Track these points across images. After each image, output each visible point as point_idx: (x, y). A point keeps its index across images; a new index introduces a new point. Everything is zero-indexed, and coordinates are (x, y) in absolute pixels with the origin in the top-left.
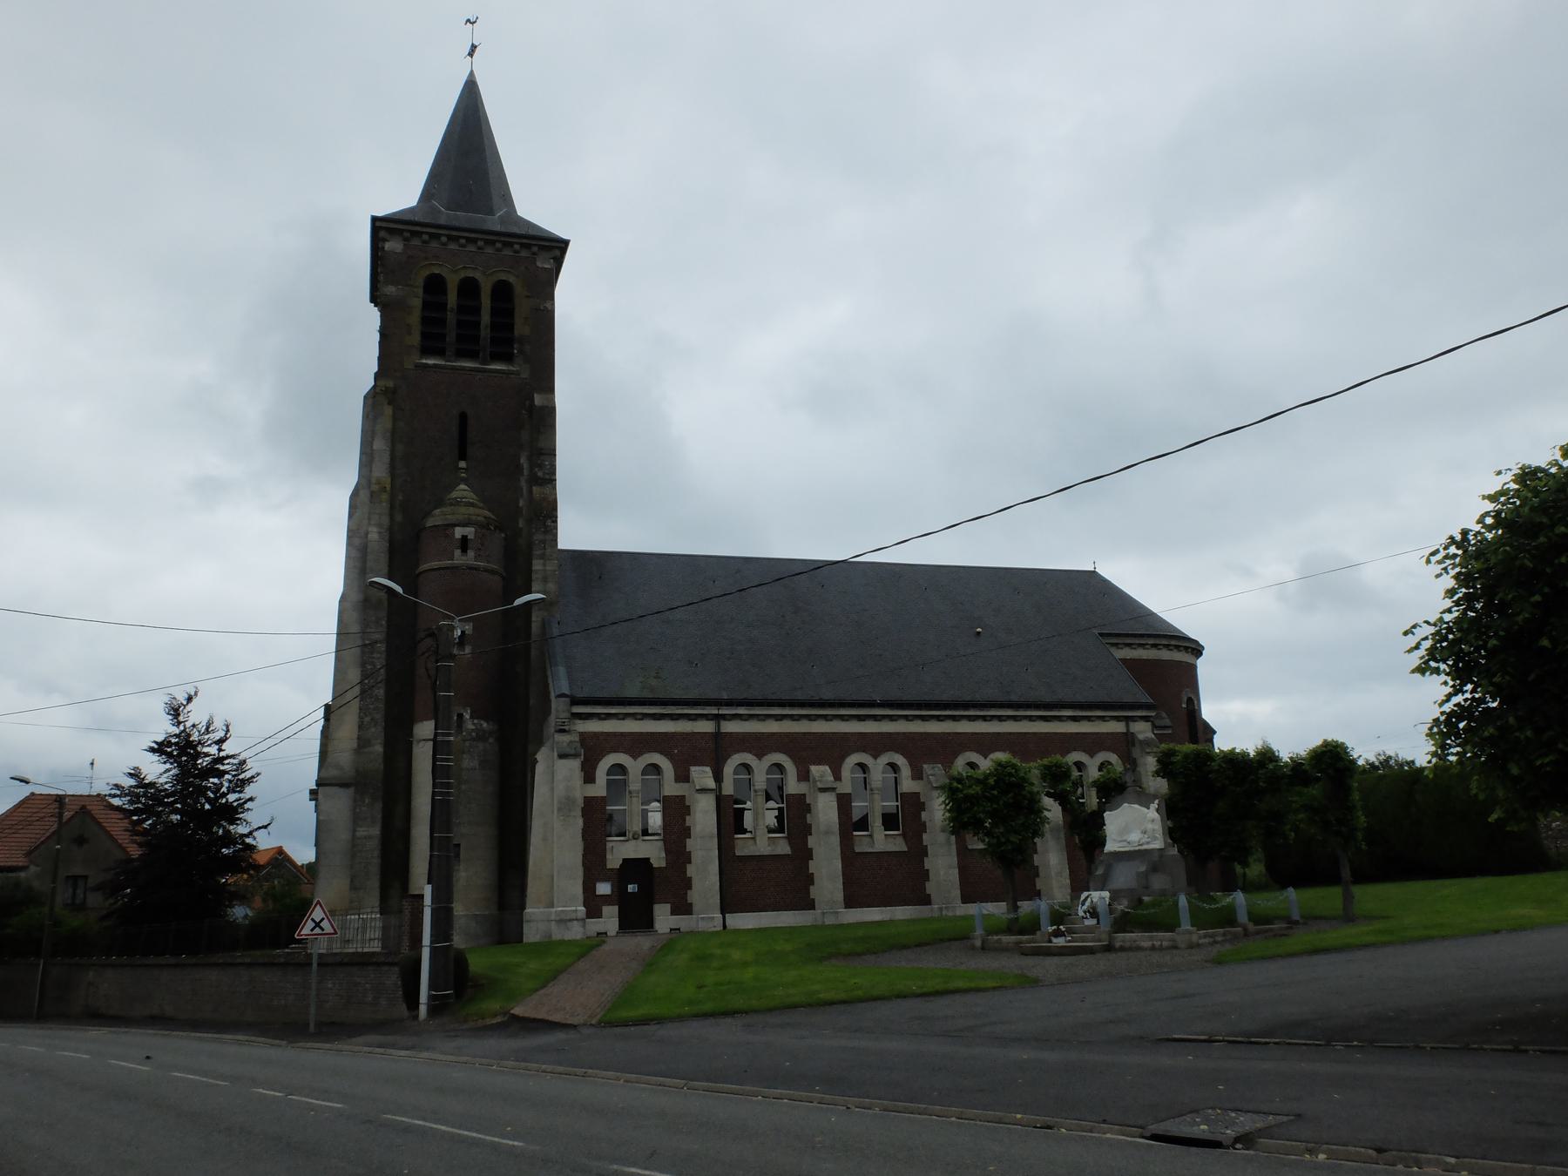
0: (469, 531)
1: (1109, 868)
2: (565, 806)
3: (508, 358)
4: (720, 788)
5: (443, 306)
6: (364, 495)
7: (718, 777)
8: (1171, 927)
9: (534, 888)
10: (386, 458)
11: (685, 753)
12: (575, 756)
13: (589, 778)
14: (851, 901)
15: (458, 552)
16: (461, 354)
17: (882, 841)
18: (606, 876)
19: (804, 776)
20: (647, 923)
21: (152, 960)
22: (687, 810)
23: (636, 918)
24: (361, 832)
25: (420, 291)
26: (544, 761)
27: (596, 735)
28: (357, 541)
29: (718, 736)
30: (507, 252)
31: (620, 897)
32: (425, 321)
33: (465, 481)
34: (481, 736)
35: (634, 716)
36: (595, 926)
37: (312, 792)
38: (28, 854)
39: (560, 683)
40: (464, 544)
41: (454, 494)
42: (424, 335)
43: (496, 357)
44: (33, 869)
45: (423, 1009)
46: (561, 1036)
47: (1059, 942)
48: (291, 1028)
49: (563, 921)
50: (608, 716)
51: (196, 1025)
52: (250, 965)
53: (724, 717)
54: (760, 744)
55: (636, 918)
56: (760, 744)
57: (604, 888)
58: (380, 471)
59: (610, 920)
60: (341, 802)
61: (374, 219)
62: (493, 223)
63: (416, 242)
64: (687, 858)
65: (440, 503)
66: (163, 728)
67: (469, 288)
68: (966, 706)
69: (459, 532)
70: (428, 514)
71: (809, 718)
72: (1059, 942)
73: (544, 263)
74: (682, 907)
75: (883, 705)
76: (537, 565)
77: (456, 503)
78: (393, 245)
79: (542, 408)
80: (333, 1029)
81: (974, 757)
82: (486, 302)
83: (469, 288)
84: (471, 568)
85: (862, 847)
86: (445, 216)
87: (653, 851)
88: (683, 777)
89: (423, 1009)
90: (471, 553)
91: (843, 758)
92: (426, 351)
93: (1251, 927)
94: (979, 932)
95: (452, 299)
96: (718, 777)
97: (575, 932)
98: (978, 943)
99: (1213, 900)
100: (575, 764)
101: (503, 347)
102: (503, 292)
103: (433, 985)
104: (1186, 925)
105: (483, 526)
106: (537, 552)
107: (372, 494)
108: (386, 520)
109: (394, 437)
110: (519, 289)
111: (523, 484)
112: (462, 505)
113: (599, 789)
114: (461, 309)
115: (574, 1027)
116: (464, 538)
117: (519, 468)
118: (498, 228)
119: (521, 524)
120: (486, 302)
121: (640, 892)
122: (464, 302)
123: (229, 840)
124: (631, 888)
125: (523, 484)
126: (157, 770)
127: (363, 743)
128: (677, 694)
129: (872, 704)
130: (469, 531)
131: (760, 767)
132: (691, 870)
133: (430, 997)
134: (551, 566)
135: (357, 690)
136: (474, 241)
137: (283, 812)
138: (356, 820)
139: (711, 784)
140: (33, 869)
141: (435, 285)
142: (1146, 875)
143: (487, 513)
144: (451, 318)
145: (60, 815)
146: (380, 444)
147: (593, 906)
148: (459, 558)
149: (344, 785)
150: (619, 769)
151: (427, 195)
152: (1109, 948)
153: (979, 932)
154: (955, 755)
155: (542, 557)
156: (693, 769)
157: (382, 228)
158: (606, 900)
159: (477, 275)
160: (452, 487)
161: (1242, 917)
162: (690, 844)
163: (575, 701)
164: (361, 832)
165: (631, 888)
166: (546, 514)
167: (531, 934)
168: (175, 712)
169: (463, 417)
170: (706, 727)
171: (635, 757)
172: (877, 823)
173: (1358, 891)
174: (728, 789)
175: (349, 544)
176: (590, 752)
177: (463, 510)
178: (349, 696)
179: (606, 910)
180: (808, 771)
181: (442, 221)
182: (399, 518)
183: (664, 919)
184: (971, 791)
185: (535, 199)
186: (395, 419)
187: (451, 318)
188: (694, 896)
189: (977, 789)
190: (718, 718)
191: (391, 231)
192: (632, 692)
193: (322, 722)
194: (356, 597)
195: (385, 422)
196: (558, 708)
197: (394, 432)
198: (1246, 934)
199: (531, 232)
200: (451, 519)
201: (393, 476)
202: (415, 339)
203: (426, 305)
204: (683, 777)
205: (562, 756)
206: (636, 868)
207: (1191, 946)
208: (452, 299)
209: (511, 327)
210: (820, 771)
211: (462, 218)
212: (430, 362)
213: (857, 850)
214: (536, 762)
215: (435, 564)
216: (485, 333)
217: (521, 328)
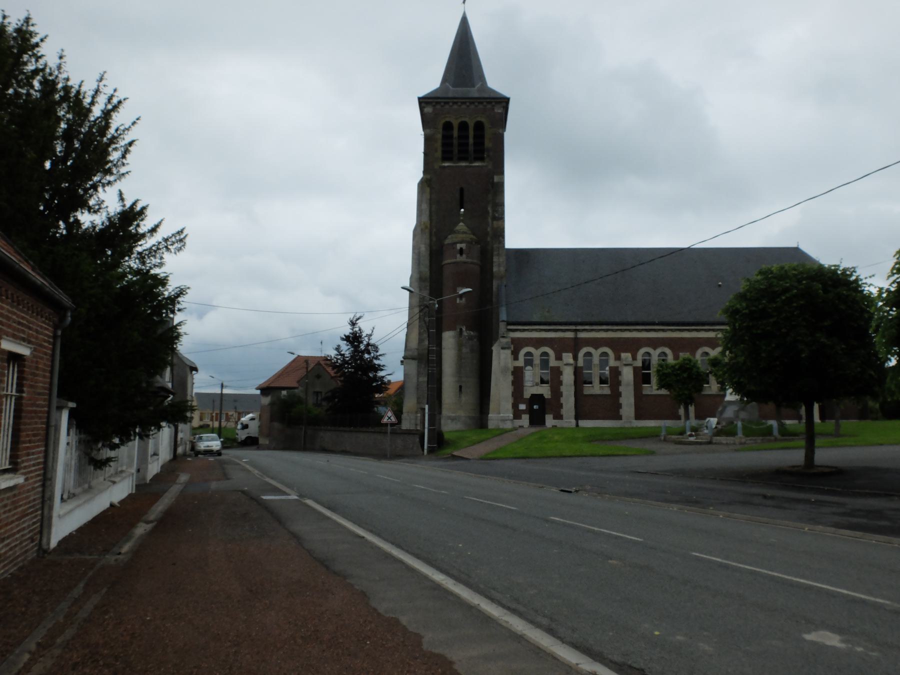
0: (463, 246)
1: (725, 408)
2: (504, 370)
3: (482, 159)
4: (576, 363)
5: (451, 137)
6: (419, 230)
7: (575, 358)
8: (734, 434)
9: (492, 406)
10: (428, 213)
11: (560, 347)
12: (508, 348)
13: (516, 358)
14: (638, 417)
15: (458, 255)
16: (461, 159)
17: (596, 389)
18: (523, 401)
19: (618, 358)
20: (542, 422)
21: (342, 428)
22: (561, 373)
23: (537, 420)
24: (421, 379)
25: (441, 130)
26: (495, 349)
27: (519, 338)
28: (417, 251)
29: (576, 339)
30: (481, 106)
31: (530, 411)
32: (444, 145)
33: (462, 221)
34: (470, 338)
35: (536, 330)
36: (518, 423)
37: (402, 362)
38: (298, 382)
39: (503, 316)
40: (461, 251)
41: (458, 228)
42: (444, 152)
43: (477, 159)
44: (300, 388)
45: (426, 451)
46: (462, 462)
47: (692, 439)
48: (381, 456)
49: (504, 420)
50: (524, 330)
51: (356, 454)
52: (374, 432)
53: (578, 330)
54: (596, 343)
55: (537, 420)
56: (596, 343)
57: (522, 407)
58: (426, 218)
59: (525, 420)
60: (413, 364)
61: (419, 99)
62: (474, 92)
63: (438, 107)
64: (561, 394)
65: (452, 232)
66: (347, 330)
67: (463, 126)
68: (703, 324)
69: (459, 246)
70: (446, 238)
71: (621, 330)
72: (692, 439)
73: (499, 110)
74: (558, 416)
75: (658, 324)
76: (495, 259)
77: (459, 232)
78: (429, 110)
79: (498, 183)
80: (396, 456)
81: (707, 349)
82: (471, 133)
83: (463, 126)
84: (465, 263)
85: (588, 390)
86: (453, 91)
87: (545, 391)
88: (559, 358)
89: (426, 451)
90: (464, 256)
91: (638, 350)
92: (444, 159)
93: (779, 437)
94: (663, 433)
95: (455, 133)
96: (575, 358)
97: (508, 425)
98: (662, 438)
99: (763, 424)
100: (509, 352)
101: (480, 153)
102: (479, 126)
103: (429, 442)
104: (740, 434)
105: (469, 243)
106: (495, 253)
107: (422, 230)
108: (428, 241)
109: (431, 202)
110: (487, 125)
111: (490, 220)
112: (461, 234)
113: (520, 363)
114: (460, 137)
115: (467, 459)
116: (461, 249)
117: (488, 212)
118: (476, 95)
119: (489, 239)
120: (471, 133)
121: (539, 410)
122: (465, 132)
123: (375, 379)
124: (535, 407)
125: (490, 220)
126: (346, 349)
127: (421, 341)
128: (556, 319)
129: (654, 324)
130: (463, 246)
131: (596, 354)
132: (563, 400)
133: (428, 447)
134: (502, 259)
135: (418, 316)
136: (464, 103)
137: (393, 368)
138: (419, 374)
139: (571, 361)
140: (300, 388)
141: (448, 126)
142: (738, 411)
143: (472, 236)
144: (455, 142)
145: (307, 368)
146: (425, 206)
147: (517, 415)
148: (459, 258)
149: (413, 359)
150: (529, 354)
151: (445, 80)
152: (710, 443)
153: (663, 433)
154: (697, 348)
155: (498, 255)
156: (564, 354)
157: (424, 102)
158: (523, 412)
159: (467, 120)
160: (457, 224)
161: (776, 432)
162: (621, 389)
163: (509, 324)
164: (421, 379)
165: (535, 407)
166: (500, 234)
167: (491, 425)
168: (353, 324)
169: (462, 190)
170: (570, 335)
171: (537, 349)
172: (596, 381)
173: (843, 423)
174: (581, 363)
175: (413, 252)
176: (516, 346)
177: (460, 236)
178: (415, 318)
179: (523, 416)
180: (620, 356)
181: (450, 95)
182: (434, 239)
183: (550, 421)
184: (666, 371)
185: (496, 79)
186: (431, 194)
187: (455, 142)
188: (564, 411)
189: (669, 371)
190: (576, 331)
191: (427, 103)
192: (535, 318)
193: (406, 330)
194: (417, 276)
195: (427, 196)
196: (502, 327)
197: (430, 199)
198: (776, 440)
199: (492, 95)
200: (455, 240)
201: (431, 220)
202: (439, 154)
203: (444, 137)
204: (559, 358)
205: (503, 348)
206: (537, 398)
207: (741, 444)
208: (455, 133)
209: (483, 144)
210: (626, 356)
211: (460, 92)
212: (446, 164)
213: (644, 393)
214: (492, 351)
215: (449, 261)
216: (471, 148)
217: (488, 144)
